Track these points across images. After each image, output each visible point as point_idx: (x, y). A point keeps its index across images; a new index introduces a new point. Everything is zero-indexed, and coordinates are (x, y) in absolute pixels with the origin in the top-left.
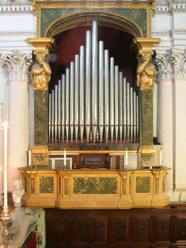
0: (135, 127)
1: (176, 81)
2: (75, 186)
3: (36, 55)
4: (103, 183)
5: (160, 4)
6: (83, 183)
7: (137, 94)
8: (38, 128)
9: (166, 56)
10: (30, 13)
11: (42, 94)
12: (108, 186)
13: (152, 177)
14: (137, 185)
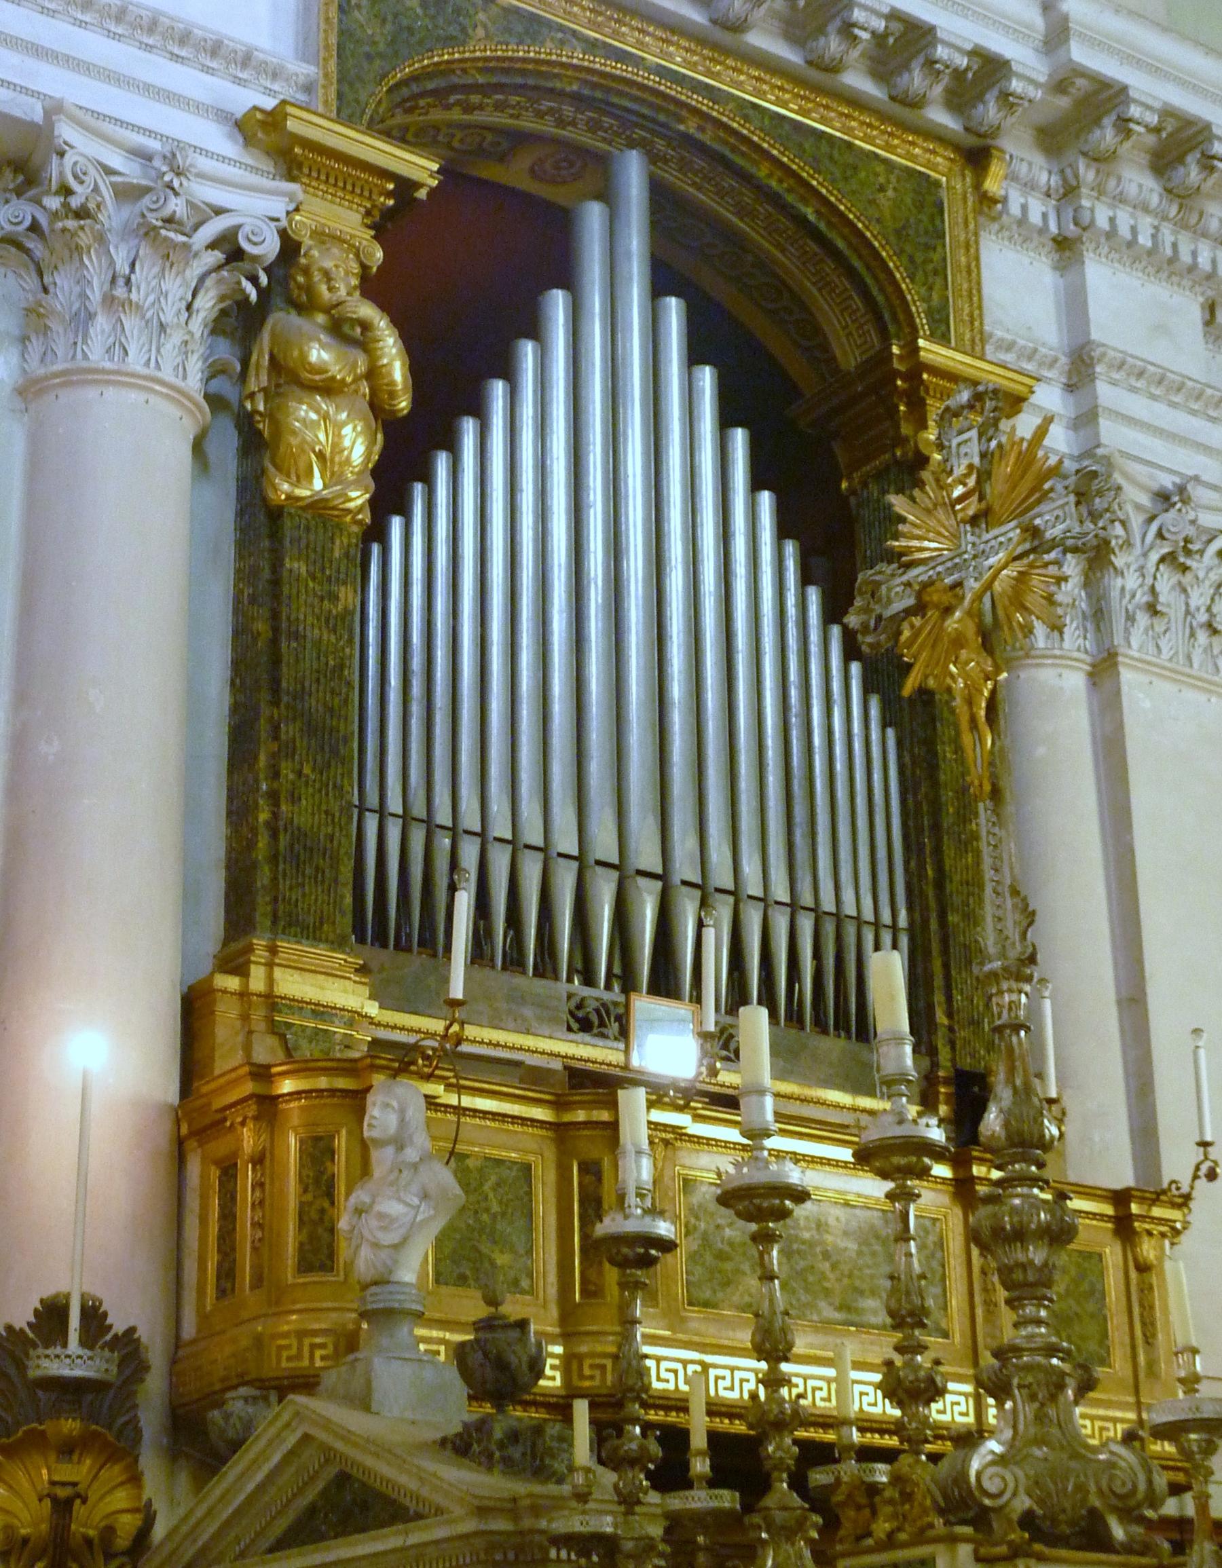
1: (1122, 670)
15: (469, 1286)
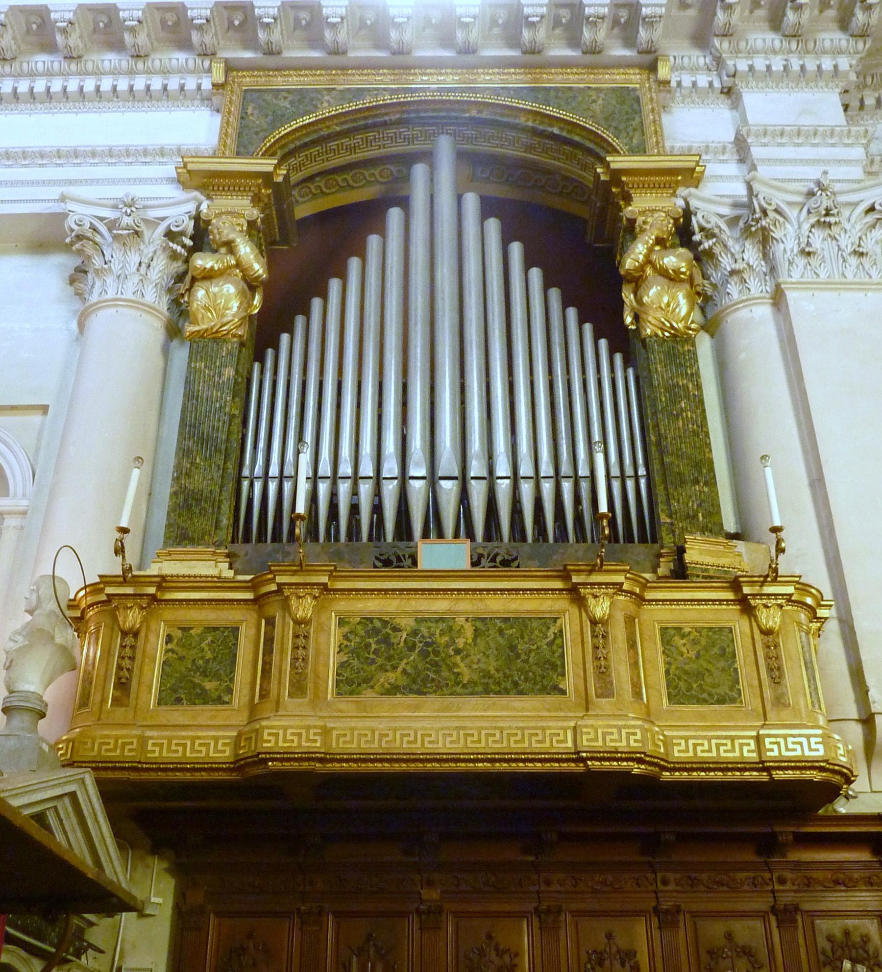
0: (630, 484)
1: (787, 292)
2: (345, 659)
3: (208, 222)
4: (492, 644)
5: (686, 65)
6: (386, 640)
7: (627, 363)
8: (188, 475)
9: (733, 222)
10: (199, 102)
11: (222, 349)
12: (518, 656)
13: (741, 626)
14: (669, 663)
15: (183, 704)
